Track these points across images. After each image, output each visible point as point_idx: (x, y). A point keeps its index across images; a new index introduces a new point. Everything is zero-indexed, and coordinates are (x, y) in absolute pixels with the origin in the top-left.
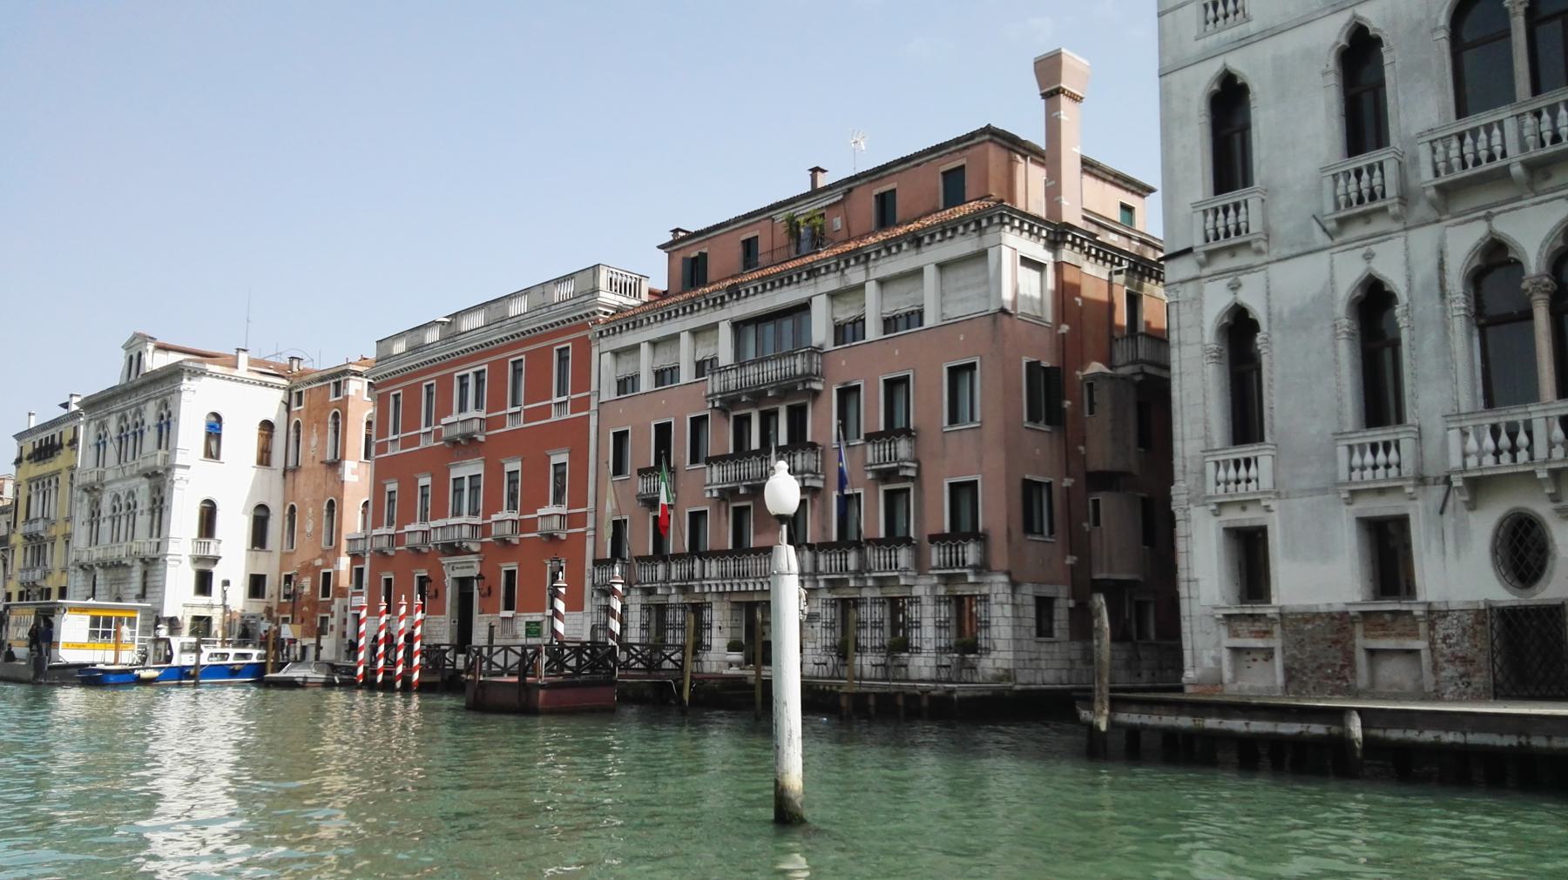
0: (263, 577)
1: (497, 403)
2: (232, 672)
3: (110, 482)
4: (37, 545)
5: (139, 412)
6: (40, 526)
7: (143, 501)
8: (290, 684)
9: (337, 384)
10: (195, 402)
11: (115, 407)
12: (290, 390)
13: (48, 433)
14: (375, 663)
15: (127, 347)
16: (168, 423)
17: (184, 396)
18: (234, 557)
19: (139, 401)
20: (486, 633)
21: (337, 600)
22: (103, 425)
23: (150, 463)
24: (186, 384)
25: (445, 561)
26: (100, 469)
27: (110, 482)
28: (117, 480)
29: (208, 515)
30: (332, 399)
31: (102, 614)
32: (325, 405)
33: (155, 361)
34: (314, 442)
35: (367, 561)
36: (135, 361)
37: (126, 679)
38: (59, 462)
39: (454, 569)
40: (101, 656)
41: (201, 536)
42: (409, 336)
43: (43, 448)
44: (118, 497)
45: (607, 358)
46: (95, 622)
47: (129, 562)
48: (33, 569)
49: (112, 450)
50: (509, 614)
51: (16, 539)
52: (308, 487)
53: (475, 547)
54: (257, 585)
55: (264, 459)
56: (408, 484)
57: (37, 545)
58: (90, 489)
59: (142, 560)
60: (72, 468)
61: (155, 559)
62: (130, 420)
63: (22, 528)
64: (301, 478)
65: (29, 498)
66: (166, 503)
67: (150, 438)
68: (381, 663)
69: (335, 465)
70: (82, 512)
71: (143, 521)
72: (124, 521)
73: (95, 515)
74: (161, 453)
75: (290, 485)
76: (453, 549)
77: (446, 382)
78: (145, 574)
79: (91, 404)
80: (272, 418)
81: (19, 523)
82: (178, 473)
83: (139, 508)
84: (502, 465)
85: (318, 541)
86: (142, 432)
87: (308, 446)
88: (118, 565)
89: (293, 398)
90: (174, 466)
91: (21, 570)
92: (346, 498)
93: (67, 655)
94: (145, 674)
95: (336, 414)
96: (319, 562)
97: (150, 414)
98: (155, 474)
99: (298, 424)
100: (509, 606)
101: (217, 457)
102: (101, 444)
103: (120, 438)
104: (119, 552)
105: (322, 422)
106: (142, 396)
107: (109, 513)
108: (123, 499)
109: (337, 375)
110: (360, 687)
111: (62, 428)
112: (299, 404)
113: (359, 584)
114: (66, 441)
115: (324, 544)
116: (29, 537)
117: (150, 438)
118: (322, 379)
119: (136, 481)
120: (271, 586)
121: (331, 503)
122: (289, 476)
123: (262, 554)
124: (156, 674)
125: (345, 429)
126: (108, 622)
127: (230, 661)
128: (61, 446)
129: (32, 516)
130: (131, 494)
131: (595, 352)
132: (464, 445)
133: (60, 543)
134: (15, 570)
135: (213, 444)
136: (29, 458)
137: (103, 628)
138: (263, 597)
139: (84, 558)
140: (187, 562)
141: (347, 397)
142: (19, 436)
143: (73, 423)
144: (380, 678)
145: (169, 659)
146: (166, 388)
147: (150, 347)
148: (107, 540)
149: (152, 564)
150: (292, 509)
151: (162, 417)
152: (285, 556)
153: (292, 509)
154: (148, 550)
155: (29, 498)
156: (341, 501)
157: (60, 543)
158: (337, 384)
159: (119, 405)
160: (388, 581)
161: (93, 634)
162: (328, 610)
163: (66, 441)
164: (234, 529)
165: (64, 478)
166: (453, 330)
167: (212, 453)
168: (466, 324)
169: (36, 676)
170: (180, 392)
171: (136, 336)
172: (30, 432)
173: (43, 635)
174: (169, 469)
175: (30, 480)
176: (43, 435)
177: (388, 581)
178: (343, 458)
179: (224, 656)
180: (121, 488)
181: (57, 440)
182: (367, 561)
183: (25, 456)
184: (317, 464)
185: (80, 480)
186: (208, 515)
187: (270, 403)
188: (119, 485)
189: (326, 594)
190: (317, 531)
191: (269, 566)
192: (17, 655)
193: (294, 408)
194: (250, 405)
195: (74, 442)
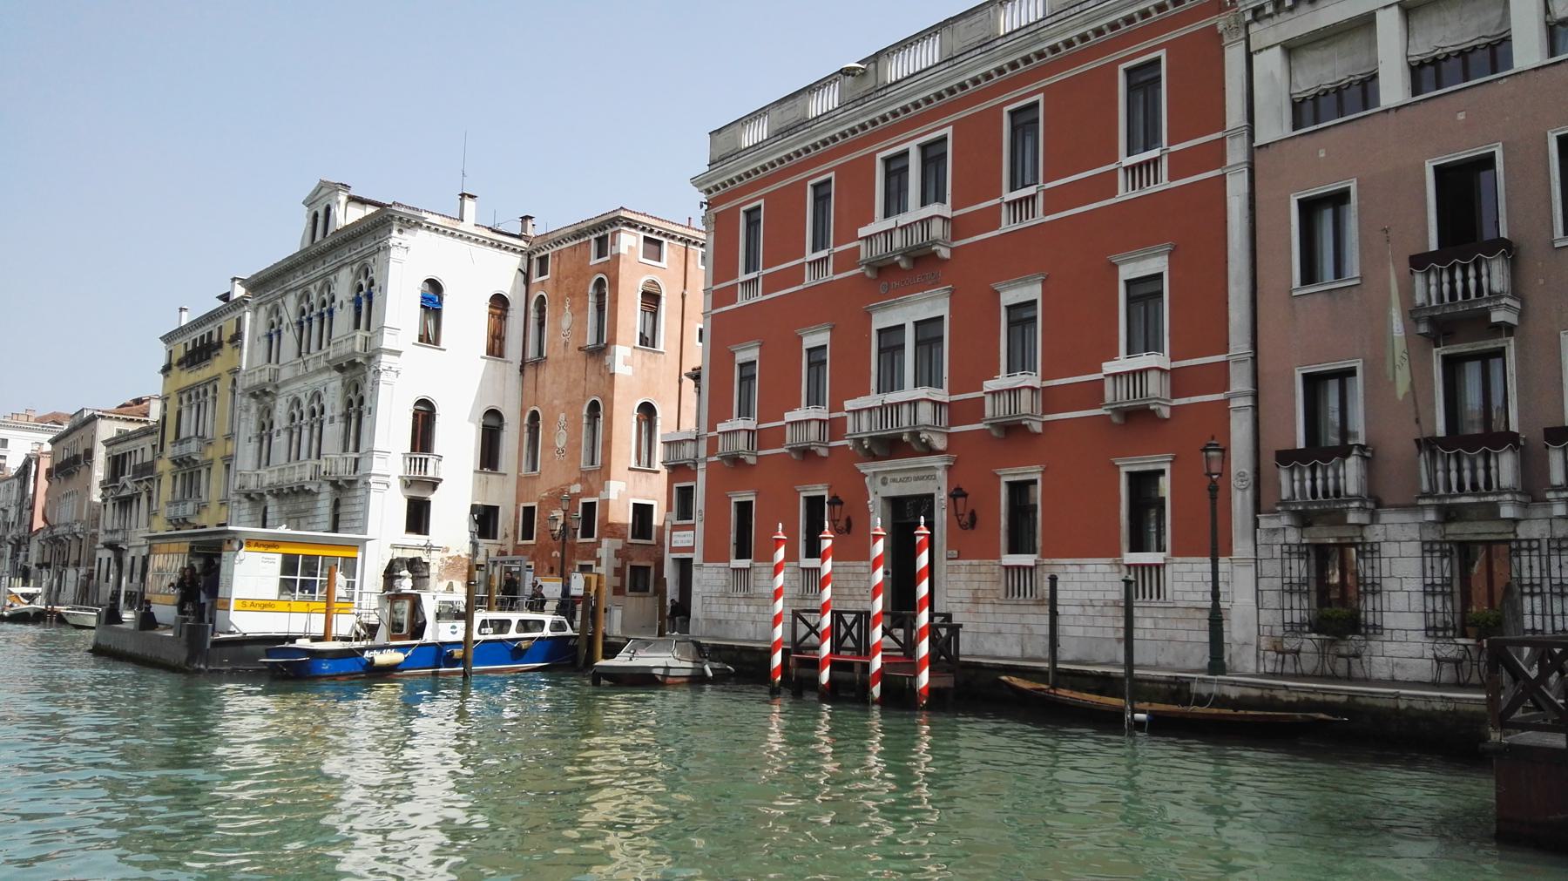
0: (496, 509)
1: (978, 184)
2: (516, 652)
3: (286, 383)
4: (189, 470)
5: (328, 286)
6: (193, 446)
7: (334, 403)
8: (643, 680)
9: (602, 242)
10: (407, 264)
11: (293, 284)
12: (529, 256)
13: (204, 331)
14: (910, 646)
15: (310, 202)
16: (370, 296)
17: (394, 253)
18: (458, 488)
19: (335, 262)
20: (1047, 585)
21: (605, 542)
22: (276, 310)
23: (345, 348)
24: (395, 237)
25: (868, 468)
26: (273, 366)
27: (286, 383)
28: (297, 379)
29: (424, 418)
30: (594, 261)
31: (302, 551)
32: (582, 271)
33: (346, 215)
34: (566, 322)
35: (701, 476)
36: (321, 218)
37: (351, 672)
38: (218, 365)
39: (885, 482)
40: (298, 622)
41: (413, 449)
42: (775, 113)
43: (198, 349)
44: (297, 402)
45: (1270, 64)
46: (289, 565)
47: (314, 488)
48: (184, 502)
49: (289, 339)
50: (744, 563)
51: (164, 466)
52: (559, 390)
53: (940, 443)
54: (485, 520)
55: (496, 348)
56: (781, 348)
57: (189, 470)
58: (261, 394)
59: (334, 484)
60: (235, 371)
61: (351, 483)
62: (314, 300)
63: (170, 451)
64: (547, 374)
65: (179, 414)
66: (367, 403)
67: (343, 318)
68: (924, 648)
69: (600, 351)
70: (248, 426)
71: (333, 432)
72: (305, 433)
73: (265, 430)
74: (361, 334)
75: (530, 384)
76: (891, 446)
77: (858, 175)
78: (337, 504)
79: (259, 284)
80: (506, 291)
81: (167, 446)
82: (385, 361)
83: (328, 413)
84: (997, 294)
85: (575, 458)
86: (331, 312)
87: (558, 329)
88: (299, 492)
89: (536, 261)
90: (380, 351)
91: (168, 503)
92: (617, 398)
93: (245, 623)
94: (382, 658)
95: (600, 283)
96: (576, 489)
97: (343, 286)
98: (353, 364)
99: (541, 301)
100: (743, 553)
101: (437, 342)
102: (273, 336)
103: (300, 323)
104: (303, 473)
105: (577, 294)
106: (332, 261)
107: (286, 423)
108: (305, 402)
109: (602, 226)
110: (775, 692)
111: (221, 322)
112: (542, 272)
113: (685, 510)
114: (226, 337)
115: (584, 464)
116: (179, 462)
117: (343, 318)
118: (579, 234)
119: (325, 376)
120: (507, 521)
121: (594, 407)
122: (529, 372)
123: (493, 477)
124: (399, 657)
125: (615, 301)
126: (310, 564)
127: (512, 633)
128: (220, 344)
129: (183, 435)
130: (317, 396)
131: (1234, 57)
132: (915, 266)
133: (218, 467)
134: (162, 504)
135: (431, 324)
136: (180, 363)
137: (301, 576)
138: (495, 537)
139: (252, 484)
140: (396, 484)
141: (618, 256)
142: (168, 338)
143: (237, 314)
144: (825, 676)
145: (418, 631)
146: (368, 244)
147: (343, 198)
148: (283, 459)
149: (346, 492)
150: (534, 416)
151: (360, 288)
152: (522, 481)
153: (534, 416)
154: (342, 469)
155: (179, 414)
156: (610, 403)
157: (218, 467)
158: (602, 242)
159: (300, 279)
160: (744, 508)
161: (287, 586)
162: (593, 557)
163: (226, 337)
164: (457, 441)
165: (224, 386)
166: (869, 83)
167: (430, 338)
168: (895, 70)
169: (192, 658)
170: (387, 248)
171: (323, 185)
172: (181, 331)
173: (202, 583)
174: (372, 356)
175: (181, 392)
176: (197, 334)
177: (744, 508)
178: (613, 341)
179: (503, 625)
180: (303, 389)
181: (215, 338)
182: (701, 476)
183: (174, 361)
184: (572, 350)
185: (244, 383)
186: (424, 418)
187: (504, 272)
188: (299, 385)
189: (588, 532)
190: (573, 446)
191: (503, 495)
192: (158, 618)
193: (535, 280)
194: (481, 275)
195: (237, 337)
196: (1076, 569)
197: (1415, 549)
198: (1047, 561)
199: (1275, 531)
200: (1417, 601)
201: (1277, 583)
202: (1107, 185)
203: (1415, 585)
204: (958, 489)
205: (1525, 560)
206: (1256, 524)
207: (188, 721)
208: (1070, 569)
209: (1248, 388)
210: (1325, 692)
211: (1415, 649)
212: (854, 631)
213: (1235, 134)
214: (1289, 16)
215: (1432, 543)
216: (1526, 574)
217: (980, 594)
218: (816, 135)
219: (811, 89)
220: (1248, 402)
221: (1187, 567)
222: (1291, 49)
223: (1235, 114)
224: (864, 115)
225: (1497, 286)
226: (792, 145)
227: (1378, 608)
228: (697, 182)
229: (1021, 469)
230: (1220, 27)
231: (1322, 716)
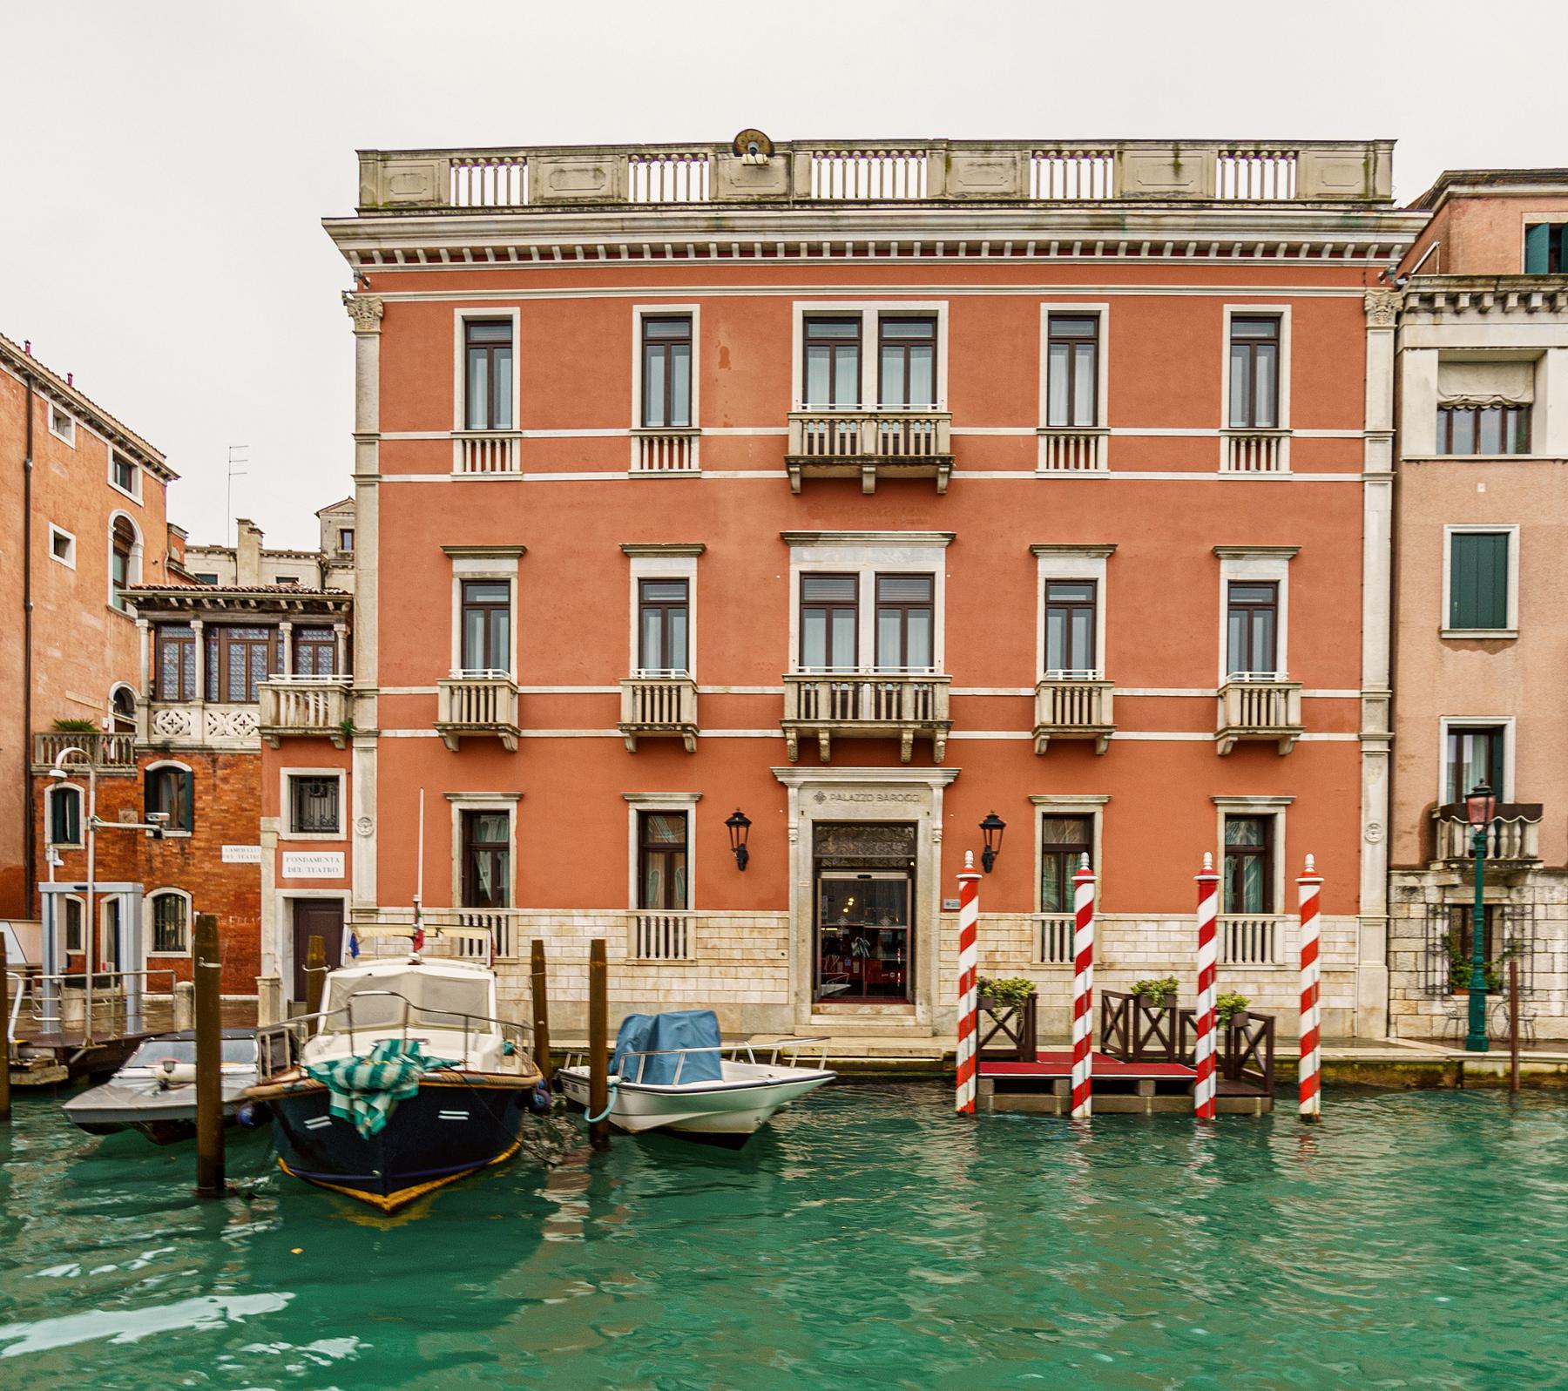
45: (1421, 369)
131: (1379, 347)
196: (1153, 926)
201: (1420, 945)
202: (1205, 455)
204: (993, 817)
207: (945, 1098)
208: (1143, 926)
209: (1382, 730)
213: (1377, 436)
217: (998, 958)
218: (667, 231)
219: (1056, 149)
220: (1382, 747)
222: (1452, 361)
223: (1378, 415)
224: (780, 230)
226: (962, 227)
228: (338, 231)
229: (1076, 798)
230: (1370, 304)
231: (502, 1158)
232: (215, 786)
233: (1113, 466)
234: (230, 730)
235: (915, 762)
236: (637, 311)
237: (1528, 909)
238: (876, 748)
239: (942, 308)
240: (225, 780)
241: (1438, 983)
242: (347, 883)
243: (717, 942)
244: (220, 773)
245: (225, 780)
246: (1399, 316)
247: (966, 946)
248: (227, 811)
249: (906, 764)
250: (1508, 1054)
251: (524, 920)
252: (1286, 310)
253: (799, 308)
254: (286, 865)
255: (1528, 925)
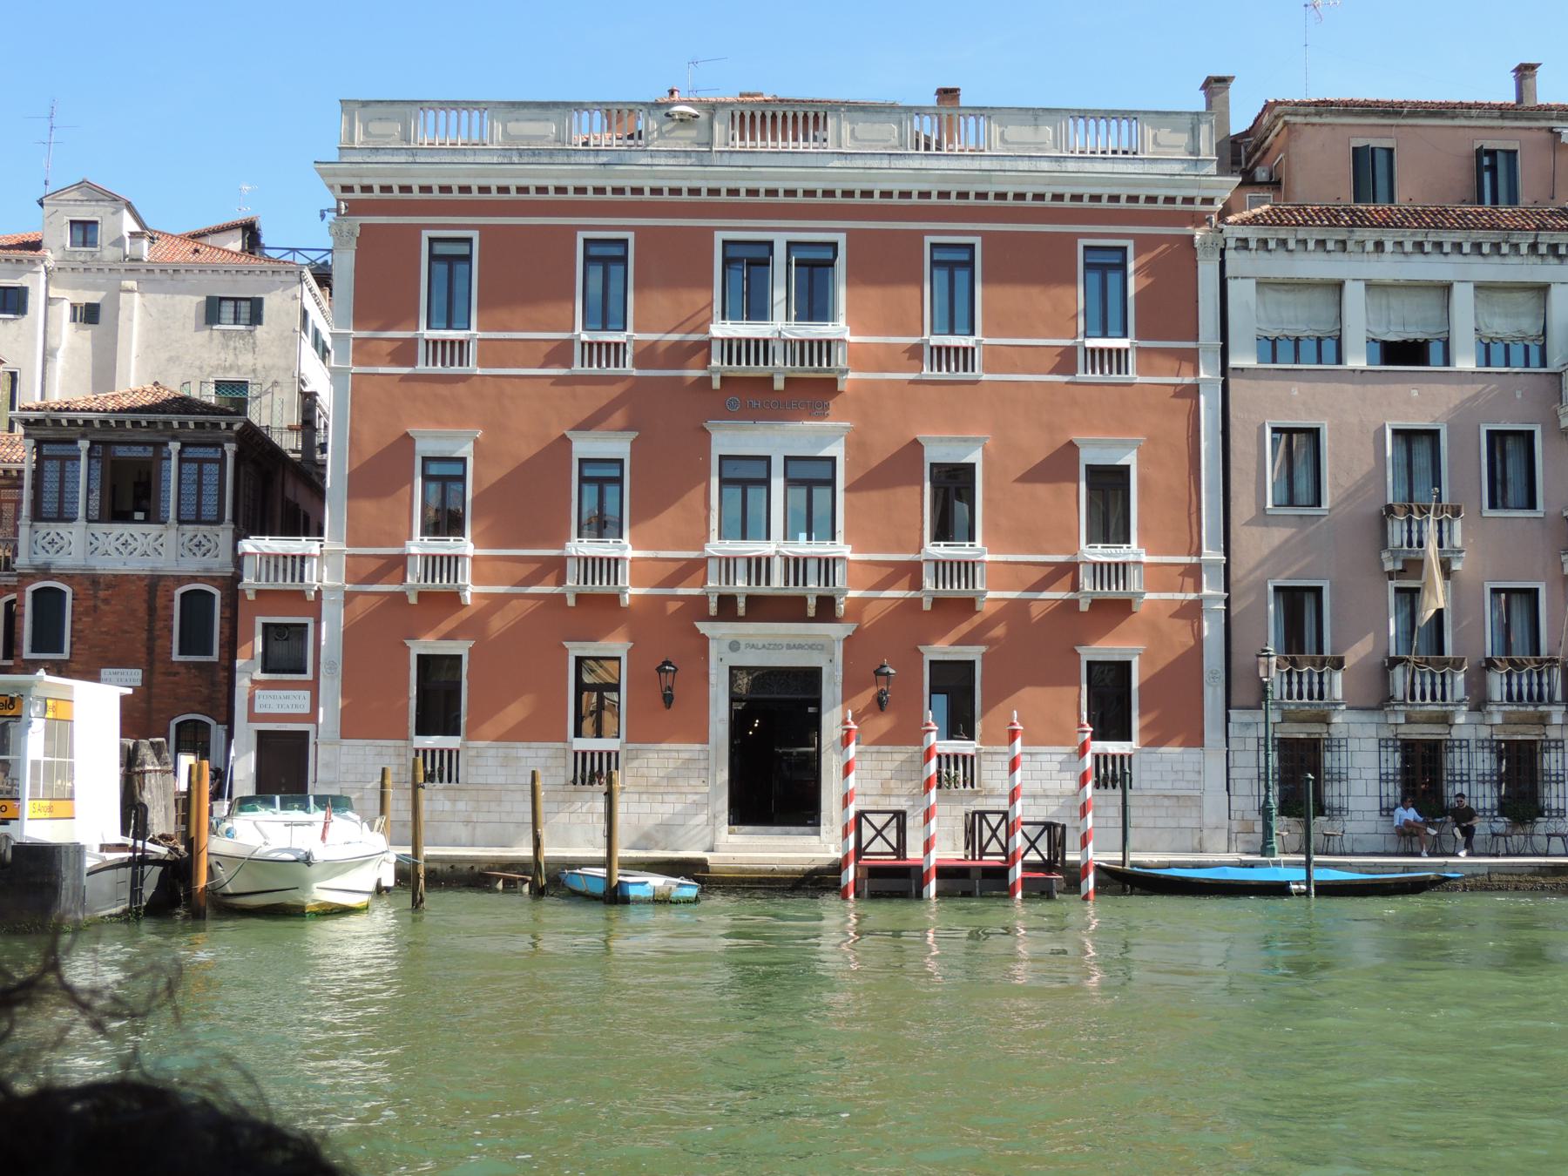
39: (737, 647)
168: (427, 132)
197: (1372, 744)
198: (470, 744)
199: (1248, 725)
200: (1374, 787)
203: (1373, 774)
205: (1457, 755)
206: (1228, 720)
210: (1407, 868)
211: (1370, 827)
212: (987, 834)
214: (1539, 260)
215: (1387, 740)
216: (1457, 766)
221: (531, 753)
225: (1458, 542)
227: (1344, 793)
232: (95, 608)
233: (986, 370)
234: (111, 550)
235: (818, 618)
236: (581, 236)
237: (1343, 743)
238: (787, 609)
239: (841, 239)
240: (106, 601)
241: (1488, 806)
242: (312, 717)
243: (646, 771)
244: (102, 594)
245: (106, 601)
246: (1222, 252)
247: (858, 776)
248: (107, 633)
249: (812, 620)
250: (1303, 858)
251: (473, 753)
252: (1130, 245)
253: (719, 237)
254: (258, 702)
255: (1343, 755)
